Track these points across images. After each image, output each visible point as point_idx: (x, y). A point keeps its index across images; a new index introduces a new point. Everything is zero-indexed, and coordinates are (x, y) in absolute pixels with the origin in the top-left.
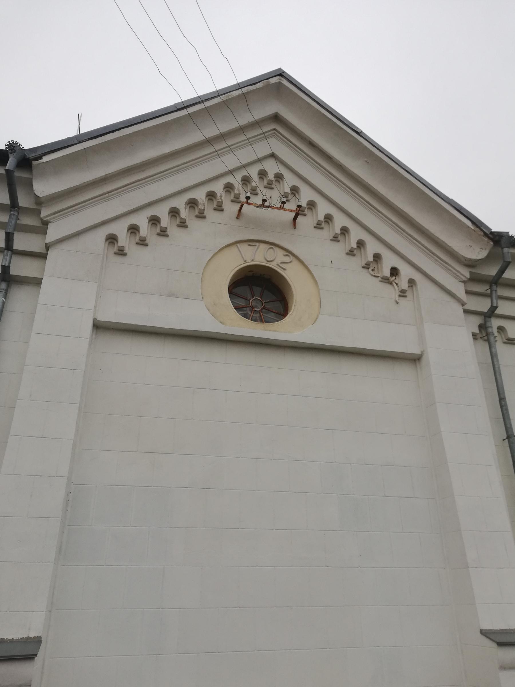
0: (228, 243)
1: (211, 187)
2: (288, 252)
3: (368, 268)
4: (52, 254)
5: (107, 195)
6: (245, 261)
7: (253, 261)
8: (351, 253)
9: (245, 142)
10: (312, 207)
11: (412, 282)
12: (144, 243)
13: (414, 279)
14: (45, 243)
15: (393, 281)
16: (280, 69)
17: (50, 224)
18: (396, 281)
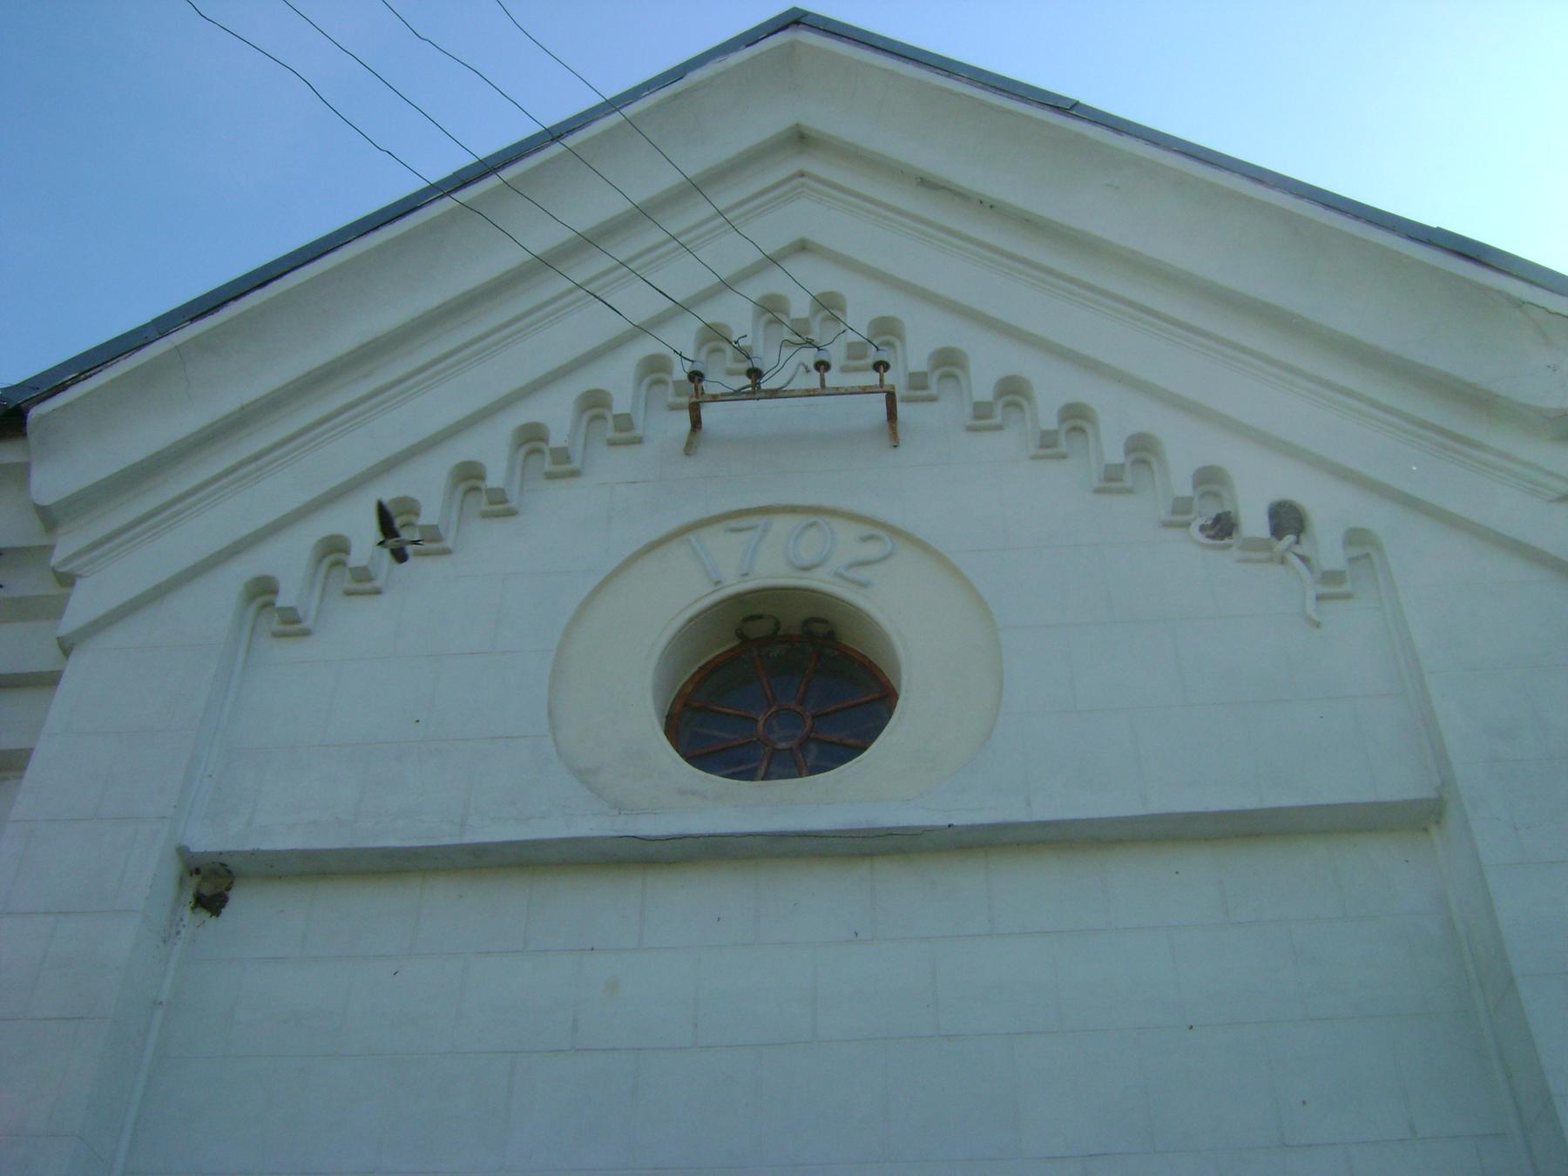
0: (655, 535)
1: (588, 380)
2: (876, 527)
3: (1188, 525)
4: (75, 672)
5: (253, 466)
6: (718, 583)
7: (746, 578)
8: (1111, 481)
9: (572, 297)
10: (956, 371)
11: (1357, 538)
12: (368, 586)
13: (1266, 519)
14: (58, 638)
15: (1288, 549)
16: (795, 10)
17: (79, 582)
18: (1298, 549)
